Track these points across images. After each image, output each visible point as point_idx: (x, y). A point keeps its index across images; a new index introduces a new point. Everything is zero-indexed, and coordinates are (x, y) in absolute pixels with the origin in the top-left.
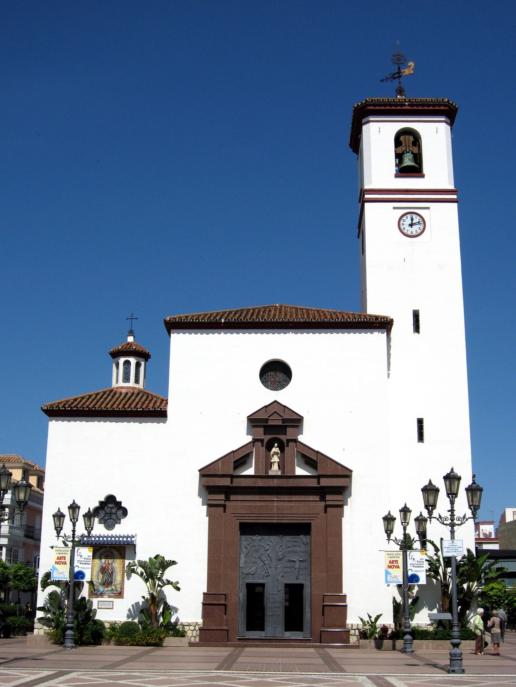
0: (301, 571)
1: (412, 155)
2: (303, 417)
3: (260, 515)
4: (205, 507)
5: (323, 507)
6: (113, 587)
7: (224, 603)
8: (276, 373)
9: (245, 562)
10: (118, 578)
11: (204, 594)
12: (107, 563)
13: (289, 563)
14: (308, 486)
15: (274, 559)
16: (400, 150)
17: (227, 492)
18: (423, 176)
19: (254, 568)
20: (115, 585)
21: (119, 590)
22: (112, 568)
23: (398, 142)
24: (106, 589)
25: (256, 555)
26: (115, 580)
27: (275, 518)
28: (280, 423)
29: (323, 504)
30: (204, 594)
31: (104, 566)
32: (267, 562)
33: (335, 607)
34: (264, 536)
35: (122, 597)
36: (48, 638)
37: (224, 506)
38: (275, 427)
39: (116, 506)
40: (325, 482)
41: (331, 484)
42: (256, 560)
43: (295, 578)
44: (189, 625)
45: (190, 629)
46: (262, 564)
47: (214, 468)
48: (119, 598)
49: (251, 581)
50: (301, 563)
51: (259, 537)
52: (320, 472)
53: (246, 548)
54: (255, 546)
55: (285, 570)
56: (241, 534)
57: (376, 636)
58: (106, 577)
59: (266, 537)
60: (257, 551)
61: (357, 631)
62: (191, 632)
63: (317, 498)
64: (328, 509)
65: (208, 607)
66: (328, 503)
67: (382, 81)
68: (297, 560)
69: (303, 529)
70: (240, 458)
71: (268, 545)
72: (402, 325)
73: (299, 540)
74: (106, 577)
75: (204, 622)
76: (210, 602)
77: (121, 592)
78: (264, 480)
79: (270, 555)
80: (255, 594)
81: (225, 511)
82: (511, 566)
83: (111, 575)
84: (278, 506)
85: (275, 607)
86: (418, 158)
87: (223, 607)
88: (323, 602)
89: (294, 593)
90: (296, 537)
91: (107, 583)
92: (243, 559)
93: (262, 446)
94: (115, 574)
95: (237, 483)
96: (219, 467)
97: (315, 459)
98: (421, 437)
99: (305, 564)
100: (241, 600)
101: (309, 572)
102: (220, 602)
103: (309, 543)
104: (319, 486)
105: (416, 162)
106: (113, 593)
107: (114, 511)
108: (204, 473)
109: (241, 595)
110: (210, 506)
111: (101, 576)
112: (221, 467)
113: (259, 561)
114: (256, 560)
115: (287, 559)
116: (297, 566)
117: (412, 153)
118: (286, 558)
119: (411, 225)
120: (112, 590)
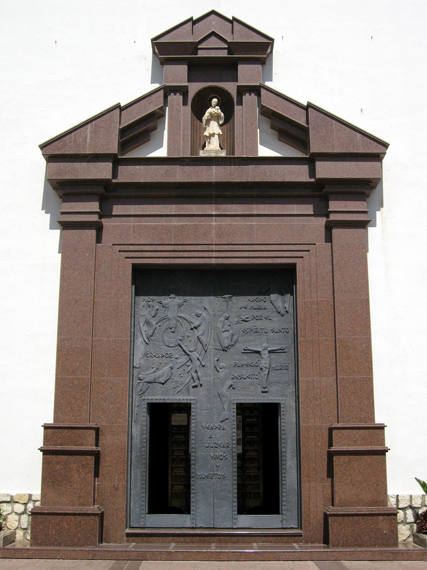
0: (273, 374)
2: (273, 40)
3: (180, 248)
4: (57, 233)
5: (323, 229)
7: (94, 448)
9: (146, 355)
13: (245, 357)
14: (287, 179)
15: (211, 347)
17: (108, 194)
19: (167, 368)
25: (171, 339)
27: (214, 254)
28: (224, 54)
29: (322, 221)
30: (46, 427)
32: (195, 355)
34: (188, 298)
37: (99, 228)
40: (326, 170)
42: (170, 351)
43: (260, 390)
44: (12, 501)
46: (184, 359)
47: (75, 141)
49: (159, 397)
50: (273, 356)
51: (178, 300)
53: (148, 323)
54: (169, 319)
55: (237, 372)
56: (137, 293)
59: (193, 300)
60: (173, 330)
61: (410, 512)
62: (17, 517)
63: (309, 209)
64: (335, 232)
65: (54, 458)
66: (333, 217)
68: (265, 349)
69: (279, 278)
70: (136, 127)
71: (198, 316)
73: (268, 305)
76: (59, 448)
78: (187, 168)
79: (203, 338)
80: (168, 427)
81: (99, 240)
84: (220, 227)
85: (217, 458)
87: (91, 460)
89: (259, 425)
90: (261, 297)
92: (140, 348)
93: (185, 103)
95: (128, 174)
96: (86, 138)
97: (302, 121)
99: (282, 359)
100: (137, 441)
101: (292, 377)
102: (82, 448)
103: (291, 310)
104: (313, 180)
108: (53, 150)
109: (136, 431)
110: (65, 226)
112: (91, 138)
113: (177, 353)
114: (170, 351)
115: (240, 346)
116: (264, 362)
118: (238, 345)
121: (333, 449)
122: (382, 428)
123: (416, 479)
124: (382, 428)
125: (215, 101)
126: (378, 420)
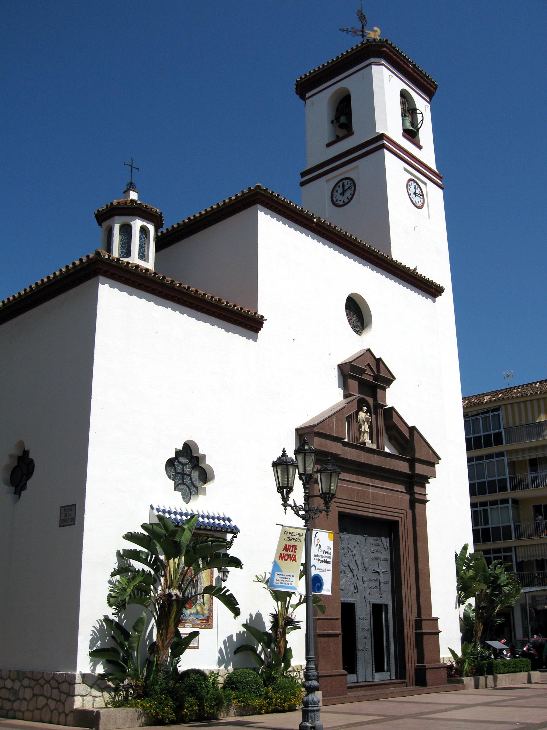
3: (358, 504)
27: (371, 510)
36: (136, 715)
39: (190, 460)
47: (329, 426)
57: (453, 675)
67: (342, 30)
76: (325, 632)
77: (208, 617)
107: (187, 470)
119: (343, 194)
120: (197, 613)
122: (436, 619)
123: (449, 649)
124: (436, 619)
126: (434, 615)
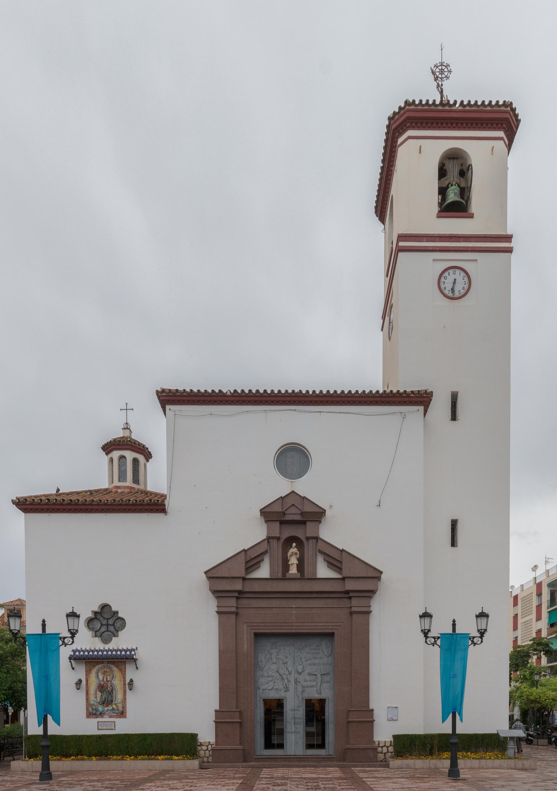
1: (458, 188)
6: (114, 706)
8: (293, 459)
10: (119, 696)
11: (216, 711)
12: (105, 680)
16: (445, 183)
18: (471, 216)
20: (115, 704)
21: (121, 709)
22: (111, 686)
23: (442, 173)
24: (106, 709)
26: (116, 698)
30: (216, 711)
31: (102, 683)
33: (362, 718)
35: (125, 717)
37: (237, 614)
38: (293, 523)
40: (350, 585)
41: (357, 586)
45: (202, 749)
48: (121, 717)
52: (346, 573)
58: (105, 696)
66: (353, 609)
70: (250, 559)
72: (440, 406)
74: (105, 696)
75: (216, 741)
76: (223, 720)
82: (556, 787)
83: (111, 693)
86: (465, 192)
88: (348, 718)
91: (107, 702)
94: (115, 692)
98: (454, 524)
105: (462, 197)
106: (114, 713)
108: (210, 575)
111: (99, 694)
117: (459, 186)
121: (349, 720)
122: (372, 710)
124: (372, 710)
125: (294, 545)
126: (371, 707)
